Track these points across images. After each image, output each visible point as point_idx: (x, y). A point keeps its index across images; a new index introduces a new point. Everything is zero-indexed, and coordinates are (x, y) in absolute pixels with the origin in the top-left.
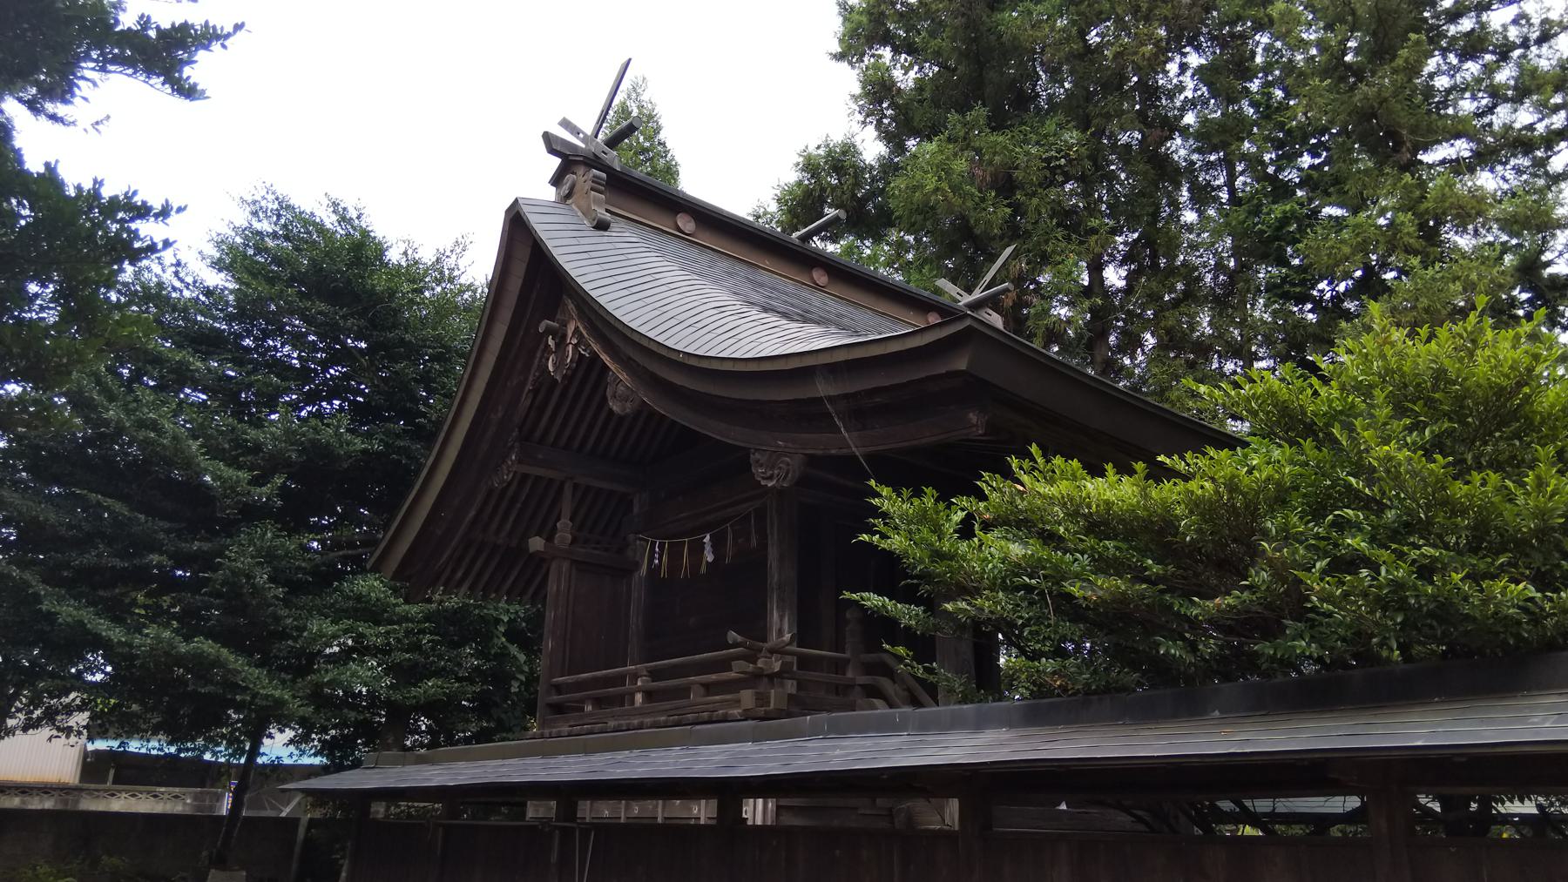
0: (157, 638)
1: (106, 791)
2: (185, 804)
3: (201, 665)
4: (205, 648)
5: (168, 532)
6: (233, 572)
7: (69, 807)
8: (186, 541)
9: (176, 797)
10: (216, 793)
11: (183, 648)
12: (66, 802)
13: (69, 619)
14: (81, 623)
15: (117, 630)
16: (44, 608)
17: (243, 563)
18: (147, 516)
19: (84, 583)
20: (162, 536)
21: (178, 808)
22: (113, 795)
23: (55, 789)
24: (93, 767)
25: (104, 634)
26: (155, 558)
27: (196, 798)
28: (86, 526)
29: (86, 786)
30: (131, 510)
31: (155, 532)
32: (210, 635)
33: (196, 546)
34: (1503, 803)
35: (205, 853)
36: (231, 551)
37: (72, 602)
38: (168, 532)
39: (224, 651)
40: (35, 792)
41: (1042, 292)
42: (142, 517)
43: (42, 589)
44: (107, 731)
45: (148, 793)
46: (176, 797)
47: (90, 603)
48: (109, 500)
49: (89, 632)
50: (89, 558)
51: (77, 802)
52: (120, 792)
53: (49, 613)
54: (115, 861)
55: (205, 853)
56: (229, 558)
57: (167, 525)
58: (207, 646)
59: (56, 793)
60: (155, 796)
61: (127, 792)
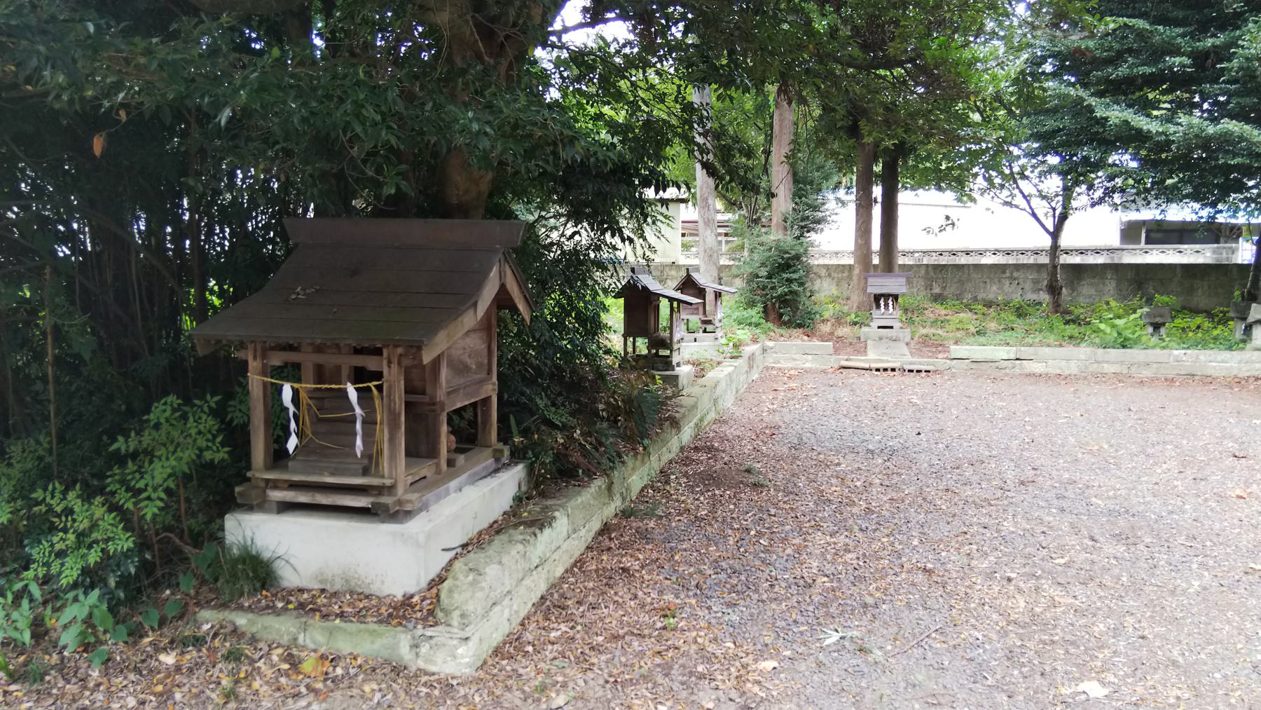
0: (1190, 126)
1: (1141, 250)
2: (1205, 257)
3: (1226, 141)
4: (1230, 127)
5: (1183, 36)
6: (1247, 59)
7: (1116, 262)
8: (1199, 40)
9: (1198, 252)
10: (1231, 248)
11: (1211, 130)
12: (1112, 258)
13: (1117, 121)
14: (1126, 122)
15: (1154, 123)
16: (1098, 115)
17: (1255, 48)
18: (1165, 26)
19: (1118, 90)
20: (1179, 40)
21: (1200, 260)
22: (1146, 252)
23: (1103, 250)
24: (1130, 232)
25: (1145, 128)
26: (1178, 60)
27: (1214, 252)
28: (1116, 46)
29: (1125, 247)
30: (1151, 24)
31: (1175, 38)
32: (1232, 117)
33: (1210, 42)
34: (161, 509)
35: (1237, 293)
36: (1244, 40)
37: (1115, 107)
38: (1183, 36)
39: (1247, 127)
40: (1089, 253)
41: (563, 220)
42: (1161, 28)
43: (1093, 101)
44: (1149, 203)
45: (1174, 249)
46: (1198, 252)
47: (1130, 106)
48: (1133, 20)
49: (1132, 128)
50: (1123, 70)
51: (1120, 258)
52: (1152, 249)
53: (1102, 118)
54: (1165, 298)
55: (1237, 293)
56: (1242, 47)
57: (1180, 30)
58: (1232, 126)
59: (1105, 253)
60: (1180, 252)
61: (1157, 249)
